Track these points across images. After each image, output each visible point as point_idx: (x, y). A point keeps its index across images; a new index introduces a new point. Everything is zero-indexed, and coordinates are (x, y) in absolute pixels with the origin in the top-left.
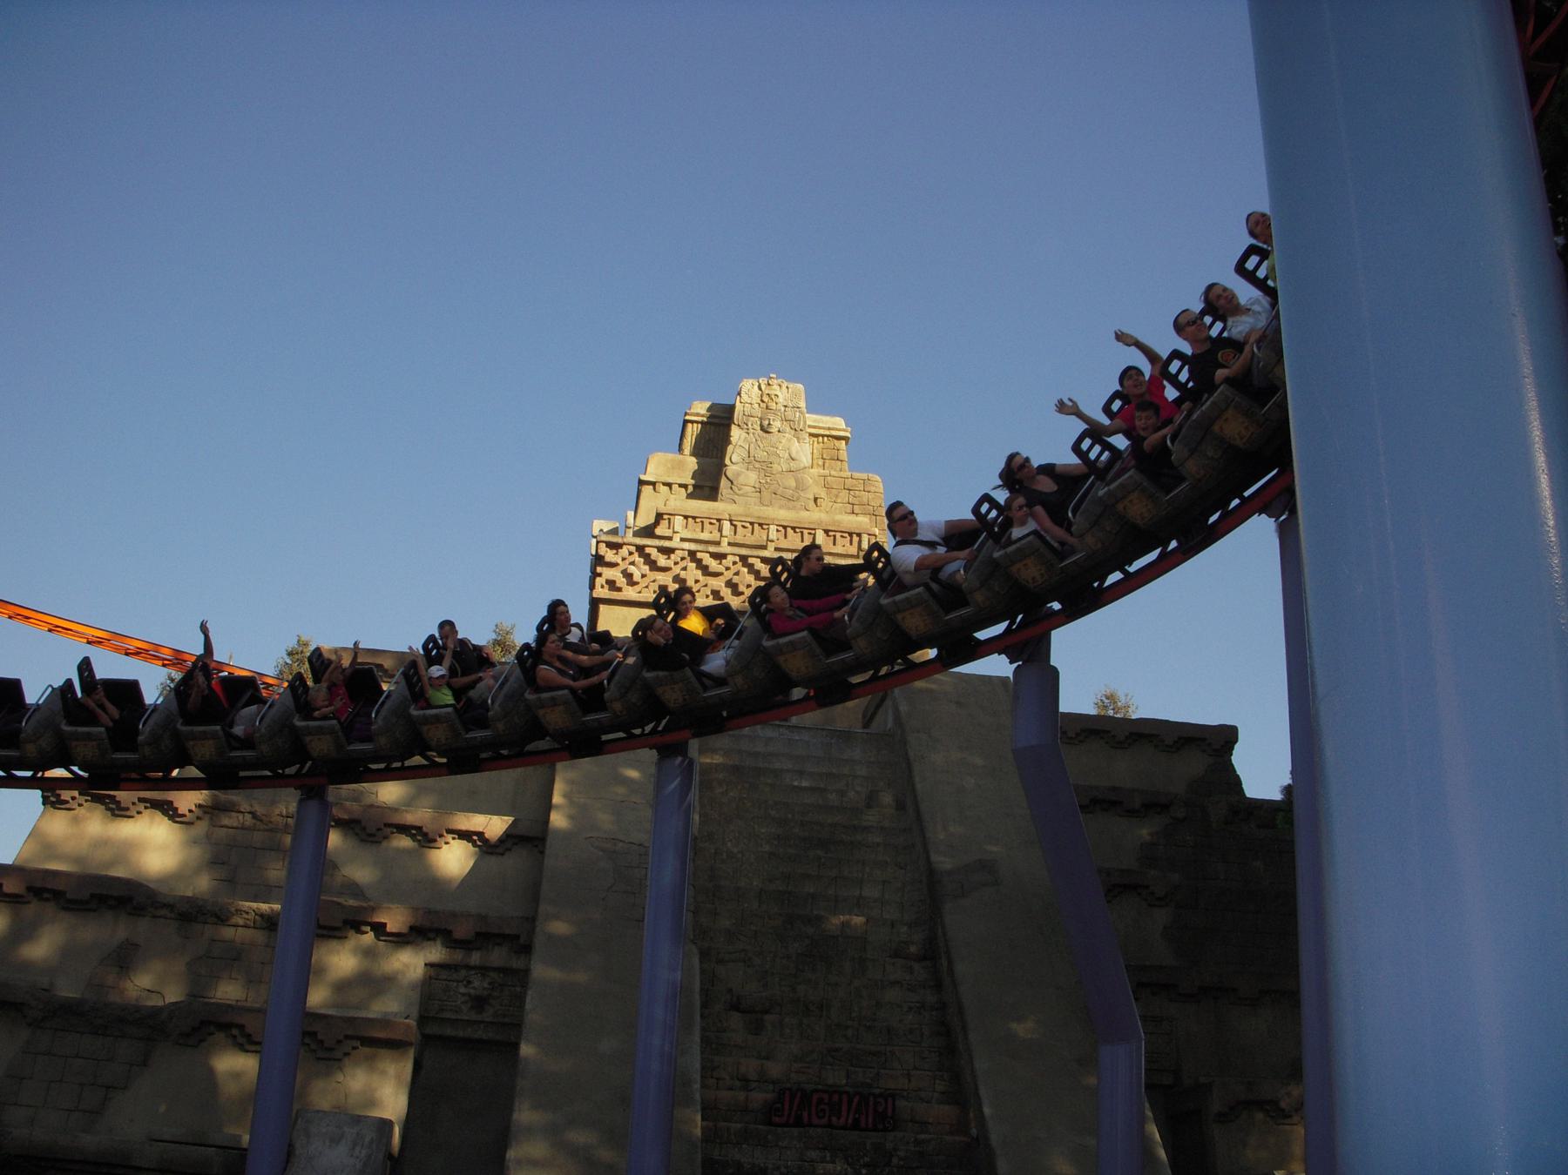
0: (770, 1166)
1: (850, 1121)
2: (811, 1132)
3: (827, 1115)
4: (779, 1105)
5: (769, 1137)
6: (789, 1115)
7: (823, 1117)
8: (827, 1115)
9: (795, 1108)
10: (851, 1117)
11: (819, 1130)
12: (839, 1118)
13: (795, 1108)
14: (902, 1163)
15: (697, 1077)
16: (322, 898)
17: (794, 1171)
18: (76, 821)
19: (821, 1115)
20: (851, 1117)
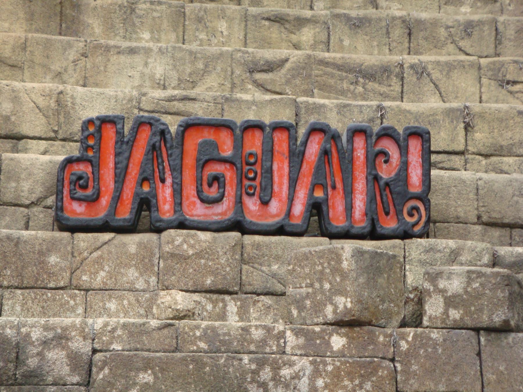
0: (36, 335)
1: (298, 209)
2: (179, 240)
3: (230, 191)
4: (82, 169)
5: (53, 259)
6: (117, 198)
7: (218, 201)
8: (230, 191)
9: (134, 172)
10: (302, 195)
11: (204, 236)
12: (265, 203)
13: (134, 172)
14: (455, 314)
15: (43, 84)
16: (317, 217)
17: (117, 346)
18: (298, 198)
19: (213, 192)
20: (302, 195)
